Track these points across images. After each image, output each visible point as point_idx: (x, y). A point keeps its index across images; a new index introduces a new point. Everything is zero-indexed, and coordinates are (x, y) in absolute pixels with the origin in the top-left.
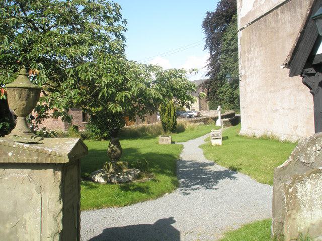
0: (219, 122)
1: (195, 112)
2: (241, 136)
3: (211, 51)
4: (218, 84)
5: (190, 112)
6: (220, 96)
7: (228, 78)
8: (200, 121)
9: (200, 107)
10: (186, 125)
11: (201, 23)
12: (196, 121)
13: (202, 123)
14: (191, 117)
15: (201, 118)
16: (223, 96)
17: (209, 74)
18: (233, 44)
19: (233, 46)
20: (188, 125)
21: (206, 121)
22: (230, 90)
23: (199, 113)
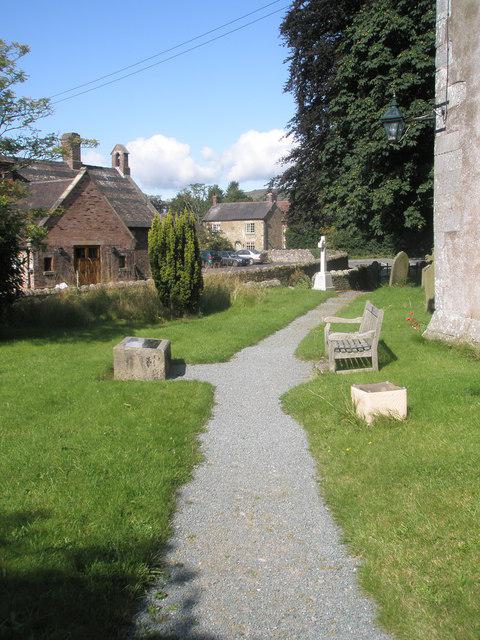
0: (320, 281)
1: (257, 253)
2: (439, 345)
3: (301, 99)
4: (323, 177)
5: (244, 252)
6: (327, 211)
7: (390, 121)
8: (270, 275)
9: (267, 245)
10: (233, 289)
11: (280, 18)
12: (260, 276)
13: (276, 281)
14: (245, 263)
15: (272, 268)
16: (334, 210)
17: (296, 154)
18: (376, 55)
19: (375, 61)
20: (239, 290)
21: (286, 274)
22: (360, 190)
23: (264, 256)
